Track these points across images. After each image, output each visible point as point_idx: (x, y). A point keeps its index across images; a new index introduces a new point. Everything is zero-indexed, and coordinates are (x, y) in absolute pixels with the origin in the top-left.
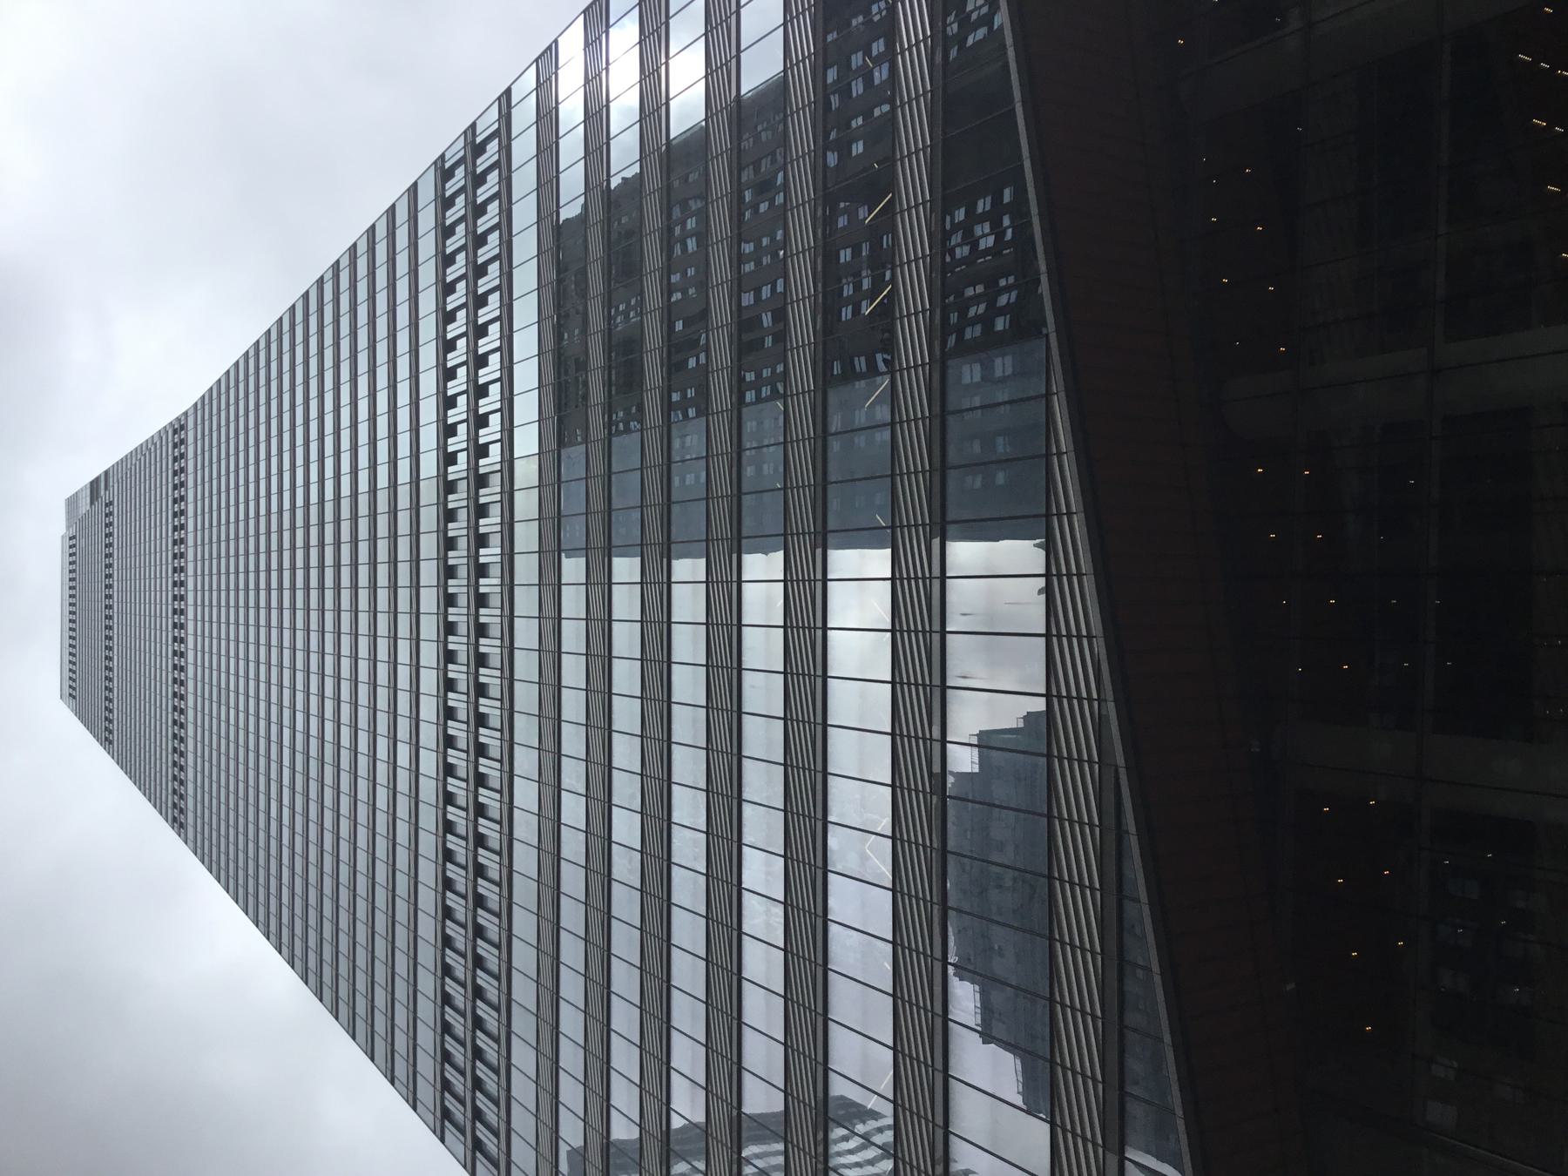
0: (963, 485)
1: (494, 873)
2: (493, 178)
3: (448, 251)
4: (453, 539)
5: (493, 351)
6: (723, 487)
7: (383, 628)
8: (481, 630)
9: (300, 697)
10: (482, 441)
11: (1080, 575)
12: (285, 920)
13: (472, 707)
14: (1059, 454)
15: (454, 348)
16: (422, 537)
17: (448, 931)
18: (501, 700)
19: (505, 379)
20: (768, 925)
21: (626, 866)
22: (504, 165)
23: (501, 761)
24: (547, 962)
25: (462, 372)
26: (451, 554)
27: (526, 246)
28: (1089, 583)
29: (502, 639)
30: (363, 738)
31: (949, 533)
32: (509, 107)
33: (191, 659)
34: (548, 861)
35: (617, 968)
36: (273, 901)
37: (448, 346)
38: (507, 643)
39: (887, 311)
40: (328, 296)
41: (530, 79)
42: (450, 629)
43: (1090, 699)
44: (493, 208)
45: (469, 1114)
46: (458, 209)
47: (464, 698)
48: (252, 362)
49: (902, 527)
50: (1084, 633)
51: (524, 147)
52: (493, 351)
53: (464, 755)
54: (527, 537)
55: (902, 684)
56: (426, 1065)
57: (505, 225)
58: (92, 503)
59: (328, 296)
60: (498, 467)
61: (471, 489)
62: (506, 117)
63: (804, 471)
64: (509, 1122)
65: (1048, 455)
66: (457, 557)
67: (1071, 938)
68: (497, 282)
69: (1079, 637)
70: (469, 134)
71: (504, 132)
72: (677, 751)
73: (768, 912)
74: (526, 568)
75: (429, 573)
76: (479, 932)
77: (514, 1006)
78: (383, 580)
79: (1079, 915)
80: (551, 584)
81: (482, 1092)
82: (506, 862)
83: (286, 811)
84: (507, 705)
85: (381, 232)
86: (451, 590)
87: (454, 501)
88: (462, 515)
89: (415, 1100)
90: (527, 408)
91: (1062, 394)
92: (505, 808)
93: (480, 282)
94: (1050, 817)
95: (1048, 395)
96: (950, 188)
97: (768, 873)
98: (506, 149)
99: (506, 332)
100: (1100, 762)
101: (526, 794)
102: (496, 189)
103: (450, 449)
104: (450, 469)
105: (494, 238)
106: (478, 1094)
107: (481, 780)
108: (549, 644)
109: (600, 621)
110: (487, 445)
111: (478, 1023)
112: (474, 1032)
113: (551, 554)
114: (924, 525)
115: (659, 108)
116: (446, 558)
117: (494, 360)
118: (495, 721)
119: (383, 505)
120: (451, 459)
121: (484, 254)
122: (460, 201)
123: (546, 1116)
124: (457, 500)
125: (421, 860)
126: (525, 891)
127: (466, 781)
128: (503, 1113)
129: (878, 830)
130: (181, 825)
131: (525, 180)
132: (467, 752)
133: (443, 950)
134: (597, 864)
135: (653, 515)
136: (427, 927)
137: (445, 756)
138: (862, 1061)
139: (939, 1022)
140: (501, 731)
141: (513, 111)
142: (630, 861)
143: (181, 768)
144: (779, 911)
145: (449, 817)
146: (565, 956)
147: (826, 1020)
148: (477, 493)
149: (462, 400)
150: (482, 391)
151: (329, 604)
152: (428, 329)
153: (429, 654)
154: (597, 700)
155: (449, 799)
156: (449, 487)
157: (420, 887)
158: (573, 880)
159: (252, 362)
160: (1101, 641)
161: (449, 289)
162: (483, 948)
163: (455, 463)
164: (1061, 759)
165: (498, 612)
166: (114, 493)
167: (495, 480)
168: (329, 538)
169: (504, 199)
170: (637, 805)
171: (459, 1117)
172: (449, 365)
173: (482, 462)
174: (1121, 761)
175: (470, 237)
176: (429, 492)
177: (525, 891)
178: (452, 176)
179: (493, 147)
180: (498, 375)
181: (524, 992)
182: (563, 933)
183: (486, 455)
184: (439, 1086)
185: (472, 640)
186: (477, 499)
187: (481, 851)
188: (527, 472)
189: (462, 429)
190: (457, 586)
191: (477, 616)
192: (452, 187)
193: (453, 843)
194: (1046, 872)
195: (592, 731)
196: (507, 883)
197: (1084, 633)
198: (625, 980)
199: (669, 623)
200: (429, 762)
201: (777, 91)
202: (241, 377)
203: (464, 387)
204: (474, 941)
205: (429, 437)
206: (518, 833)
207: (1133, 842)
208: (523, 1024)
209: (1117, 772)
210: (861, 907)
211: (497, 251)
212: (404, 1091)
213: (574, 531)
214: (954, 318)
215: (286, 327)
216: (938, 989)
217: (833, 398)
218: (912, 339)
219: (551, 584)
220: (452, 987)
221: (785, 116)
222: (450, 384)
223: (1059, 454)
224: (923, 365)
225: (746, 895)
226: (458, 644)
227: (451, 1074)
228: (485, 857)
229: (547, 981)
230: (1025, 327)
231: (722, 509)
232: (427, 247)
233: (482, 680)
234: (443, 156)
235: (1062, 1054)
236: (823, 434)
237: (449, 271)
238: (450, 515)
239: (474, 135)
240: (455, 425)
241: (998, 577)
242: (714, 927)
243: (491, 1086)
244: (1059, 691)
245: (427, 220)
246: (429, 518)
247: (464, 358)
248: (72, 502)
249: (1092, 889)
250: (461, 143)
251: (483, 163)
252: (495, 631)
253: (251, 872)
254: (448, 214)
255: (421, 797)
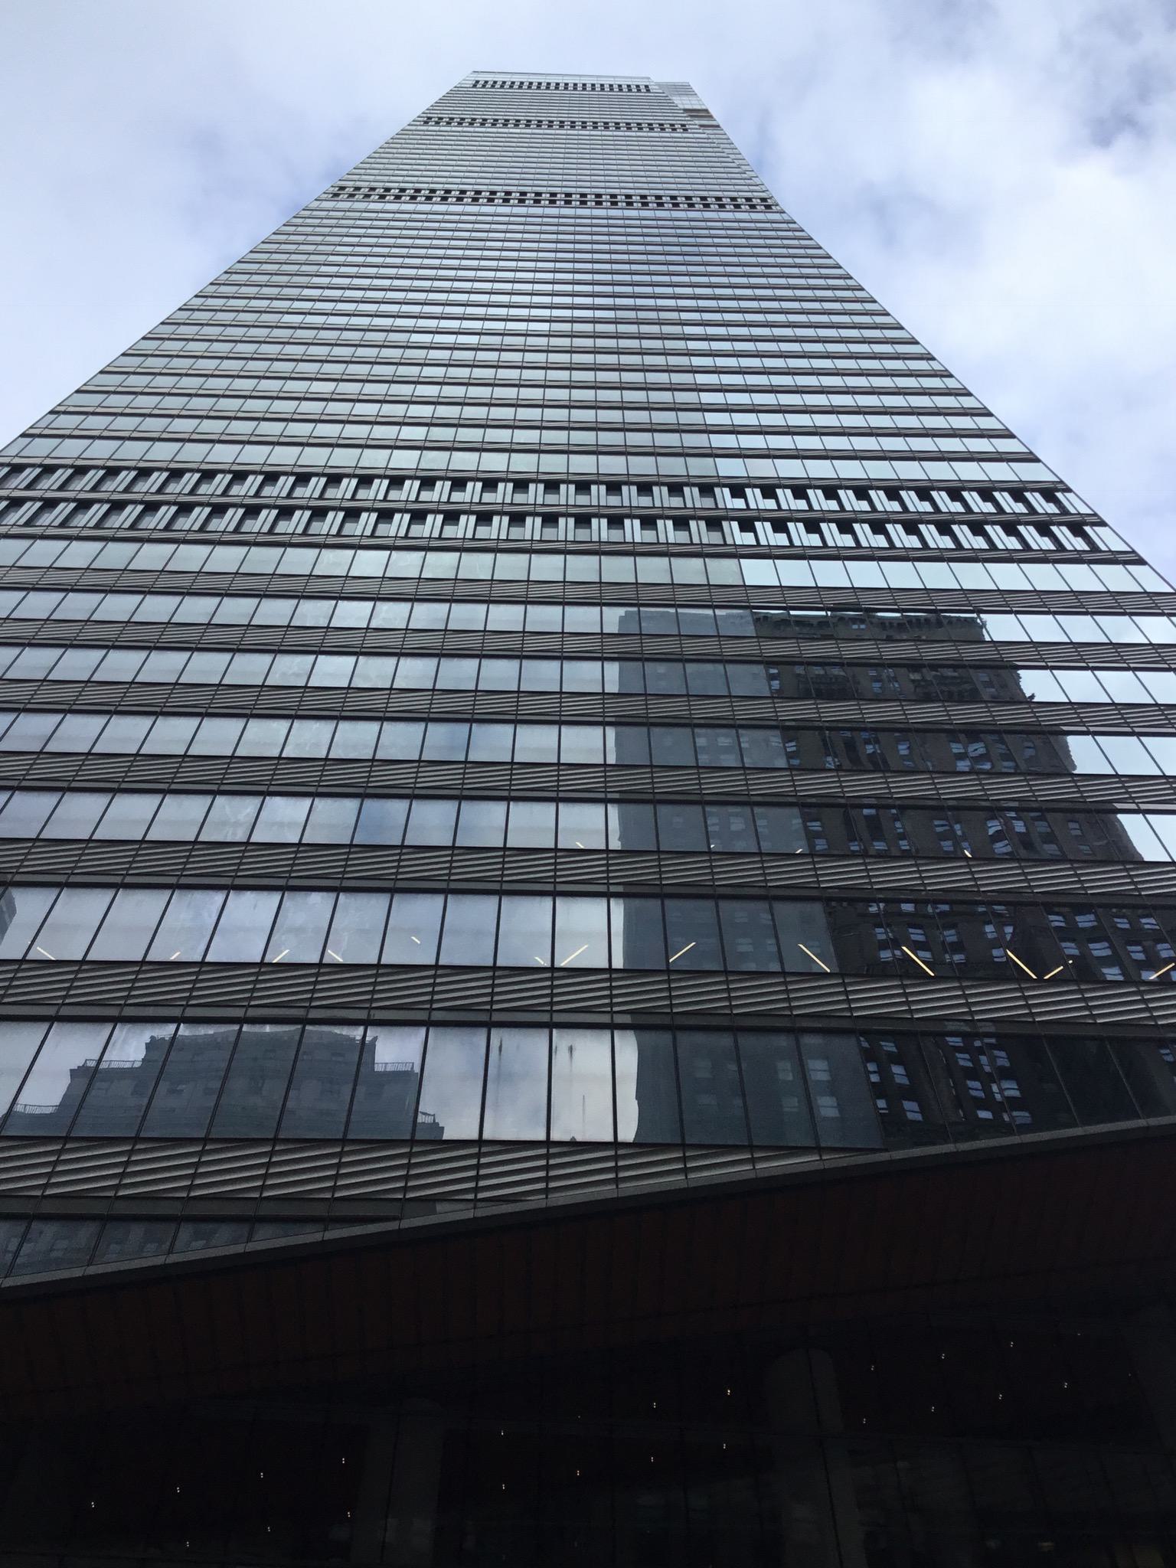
0: (703, 1054)
1: (283, 527)
2: (1013, 543)
3: (934, 494)
4: (650, 492)
5: (757, 540)
6: (713, 785)
7: (524, 414)
8: (550, 519)
9: (432, 324)
10: (758, 524)
11: (616, 1181)
12: (276, 304)
13: (466, 507)
14: (753, 1161)
15: (796, 497)
16: (623, 458)
17: (219, 477)
18: (473, 539)
19: (792, 551)
20: (224, 823)
21: (290, 669)
22: (1060, 556)
23: (406, 537)
24: (185, 582)
25: (833, 505)
26: (603, 488)
27: (973, 577)
28: (608, 1191)
29: (574, 542)
30: (431, 391)
31: (651, 1037)
32: (1125, 563)
33: (516, 210)
34: (297, 585)
35: (178, 658)
36: (253, 290)
37: (831, 491)
38: (536, 546)
39: (907, 971)
40: (914, 365)
41: (1154, 585)
42: (552, 486)
43: (476, 1190)
44: (1013, 543)
45: (49, 495)
46: (980, 506)
47: (476, 499)
48: (841, 282)
49: (669, 981)
50: (552, 1185)
51: (1081, 578)
52: (757, 540)
53: (413, 497)
54: (653, 570)
55: (552, 979)
56: (71, 450)
57: (993, 555)
58: (686, 110)
59: (914, 365)
60: (729, 541)
61: (706, 511)
62: (1114, 559)
63: (729, 874)
64: (79, 538)
65: (751, 1148)
66: (630, 496)
67: (137, 1163)
68: (898, 544)
69: (547, 1179)
70: (1094, 519)
71: (1097, 556)
72: (327, 727)
73: (237, 824)
74: (618, 569)
75: (614, 465)
76: (219, 510)
77: (135, 546)
78: (605, 416)
79: (231, 1174)
80: (599, 595)
81: (143, 512)
82: (260, 539)
83: (308, 305)
84: (468, 544)
85: (984, 423)
86: (594, 488)
87: (692, 494)
88: (676, 502)
89: (33, 436)
90: (795, 574)
91: (820, 1166)
92: (355, 541)
93: (899, 527)
94: (344, 1141)
95: (819, 1149)
96: (1029, 1046)
97: (281, 825)
98: (1077, 559)
99: (878, 553)
100: (44, 1197)
101: (370, 563)
102: (1000, 546)
103: (748, 491)
104: (726, 491)
105: (946, 542)
106: (38, 504)
107: (385, 515)
108: (535, 592)
109: (562, 649)
110: (754, 530)
111: (151, 507)
112: (107, 501)
113: (631, 596)
114: (671, 1006)
115: (1128, 725)
116: (598, 483)
117: (847, 540)
118: (417, 530)
119: (686, 418)
120: (738, 491)
121: (929, 532)
122: (1020, 508)
123: (52, 578)
124: (692, 497)
125: (267, 449)
126: (263, 560)
127: (385, 499)
128: (15, 531)
129: (329, 951)
130: (336, 195)
131: (1008, 577)
132: (448, 502)
133: (198, 471)
134: (292, 639)
135: (677, 708)
136: (224, 455)
137: (413, 478)
138: (65, 926)
139: (113, 1012)
140: (440, 538)
141: (1085, 566)
142: (297, 675)
143: (398, 197)
144: (240, 836)
145: (345, 481)
146: (112, 600)
147: (116, 886)
148: (668, 518)
149: (802, 505)
150: (780, 526)
151: (578, 358)
152: (820, 470)
153: (523, 464)
154: (474, 642)
155: (365, 481)
156: (707, 489)
157: (269, 448)
158: (275, 612)
159: (841, 282)
160: (543, 1204)
161: (893, 493)
162: (200, 514)
163: (733, 496)
164: (410, 1155)
165: (570, 538)
166: (696, 134)
167: (715, 538)
168: (650, 360)
169: (1059, 556)
170: (358, 683)
171: (45, 484)
172: (810, 492)
173: (735, 525)
174: (406, 1224)
175: (819, 515)
176: (700, 467)
177: (263, 560)
178: (1016, 500)
179: (1080, 544)
180: (797, 543)
181: (152, 556)
182: (217, 600)
183: (743, 529)
184: (79, 463)
185: (540, 510)
186: (661, 517)
187: (308, 513)
188: (723, 571)
189: (770, 504)
190: (567, 494)
191: (567, 515)
192: (1036, 499)
193: (316, 484)
194: (350, 1137)
195: (321, 633)
196: (339, 543)
197: (552, 1185)
198: (249, 669)
199: (560, 723)
200: (405, 460)
201: (1123, 854)
202: (823, 271)
203: (816, 507)
204: (208, 505)
205: (763, 469)
206: (327, 554)
207: (318, 1237)
208: (117, 555)
209: (394, 1219)
210: (246, 927)
211: (966, 545)
212: (43, 424)
213: (657, 619)
214: (889, 1047)
215: (879, 320)
216: (150, 1012)
217: (817, 908)
218: (875, 999)
219: (599, 595)
220: (157, 479)
221: (1071, 861)
222: (788, 492)
223: (753, 1161)
224: (851, 1009)
225: (256, 801)
226: (535, 494)
227: (60, 476)
228: (300, 518)
229: (164, 582)
230: (893, 1126)
231: (685, 783)
232: (969, 471)
233: (496, 519)
234: (1069, 490)
235: (145, 1151)
236: (769, 896)
237: (912, 493)
238: (614, 487)
239: (1093, 524)
240: (744, 496)
241: (589, 1090)
242: (173, 764)
243: (82, 520)
244: (555, 1155)
245: (999, 472)
246: (673, 467)
247: (848, 507)
248: (685, 90)
249: (334, 1188)
250: (1084, 510)
251: (1063, 533)
252: (550, 533)
253: (304, 268)
254: (975, 494)
255: (367, 451)
